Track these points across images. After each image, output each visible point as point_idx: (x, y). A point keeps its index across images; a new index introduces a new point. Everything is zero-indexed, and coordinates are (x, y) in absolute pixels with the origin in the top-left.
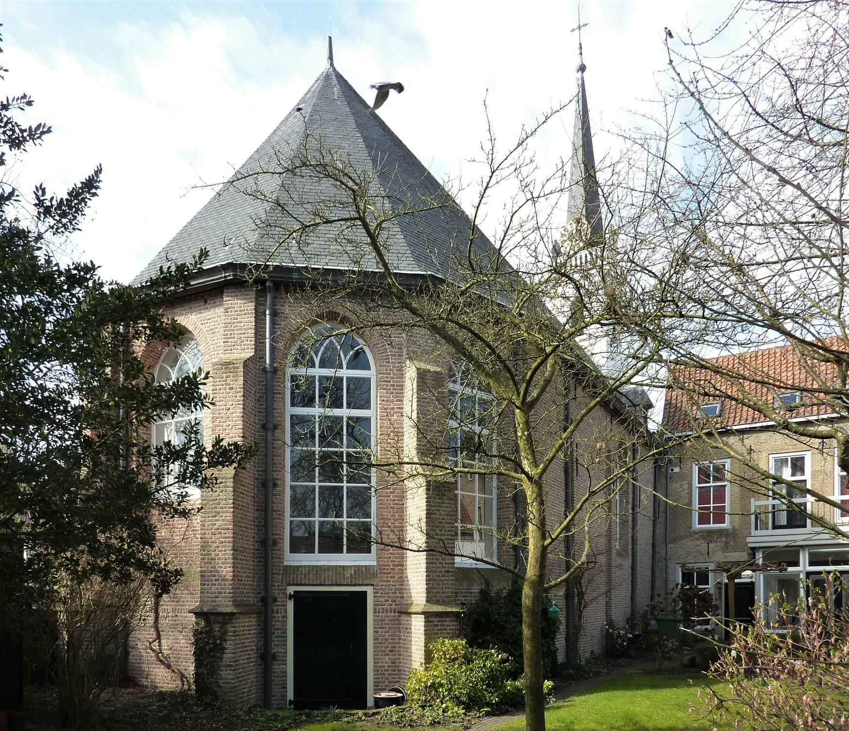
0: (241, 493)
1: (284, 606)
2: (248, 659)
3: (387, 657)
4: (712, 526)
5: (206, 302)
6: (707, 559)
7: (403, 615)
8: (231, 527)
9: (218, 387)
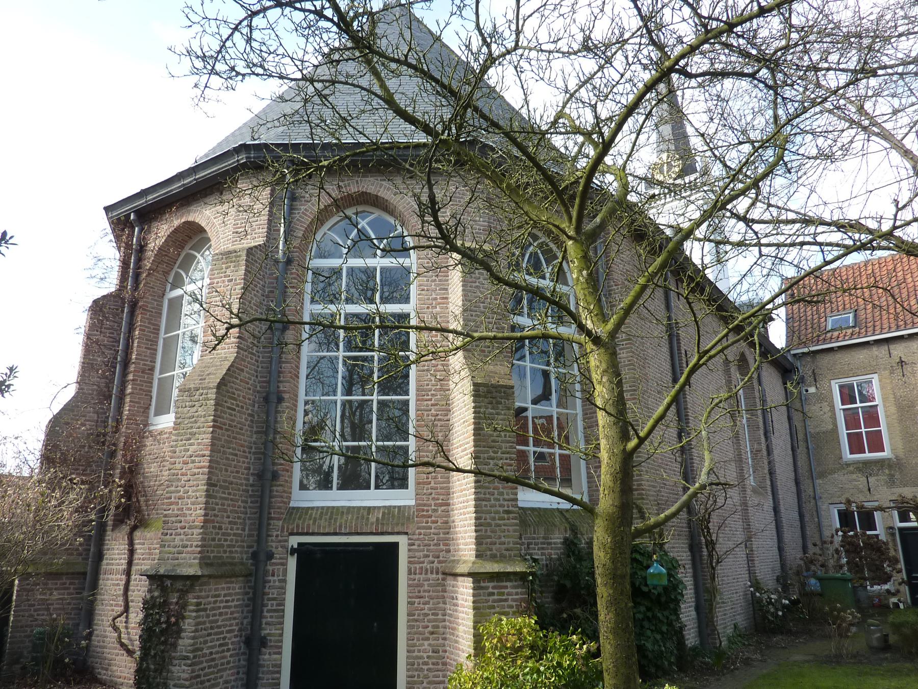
0: (229, 408)
1: (282, 564)
2: (221, 645)
3: (426, 643)
4: (868, 455)
5: (221, 194)
6: (869, 497)
7: (449, 578)
8: (208, 453)
9: (216, 281)
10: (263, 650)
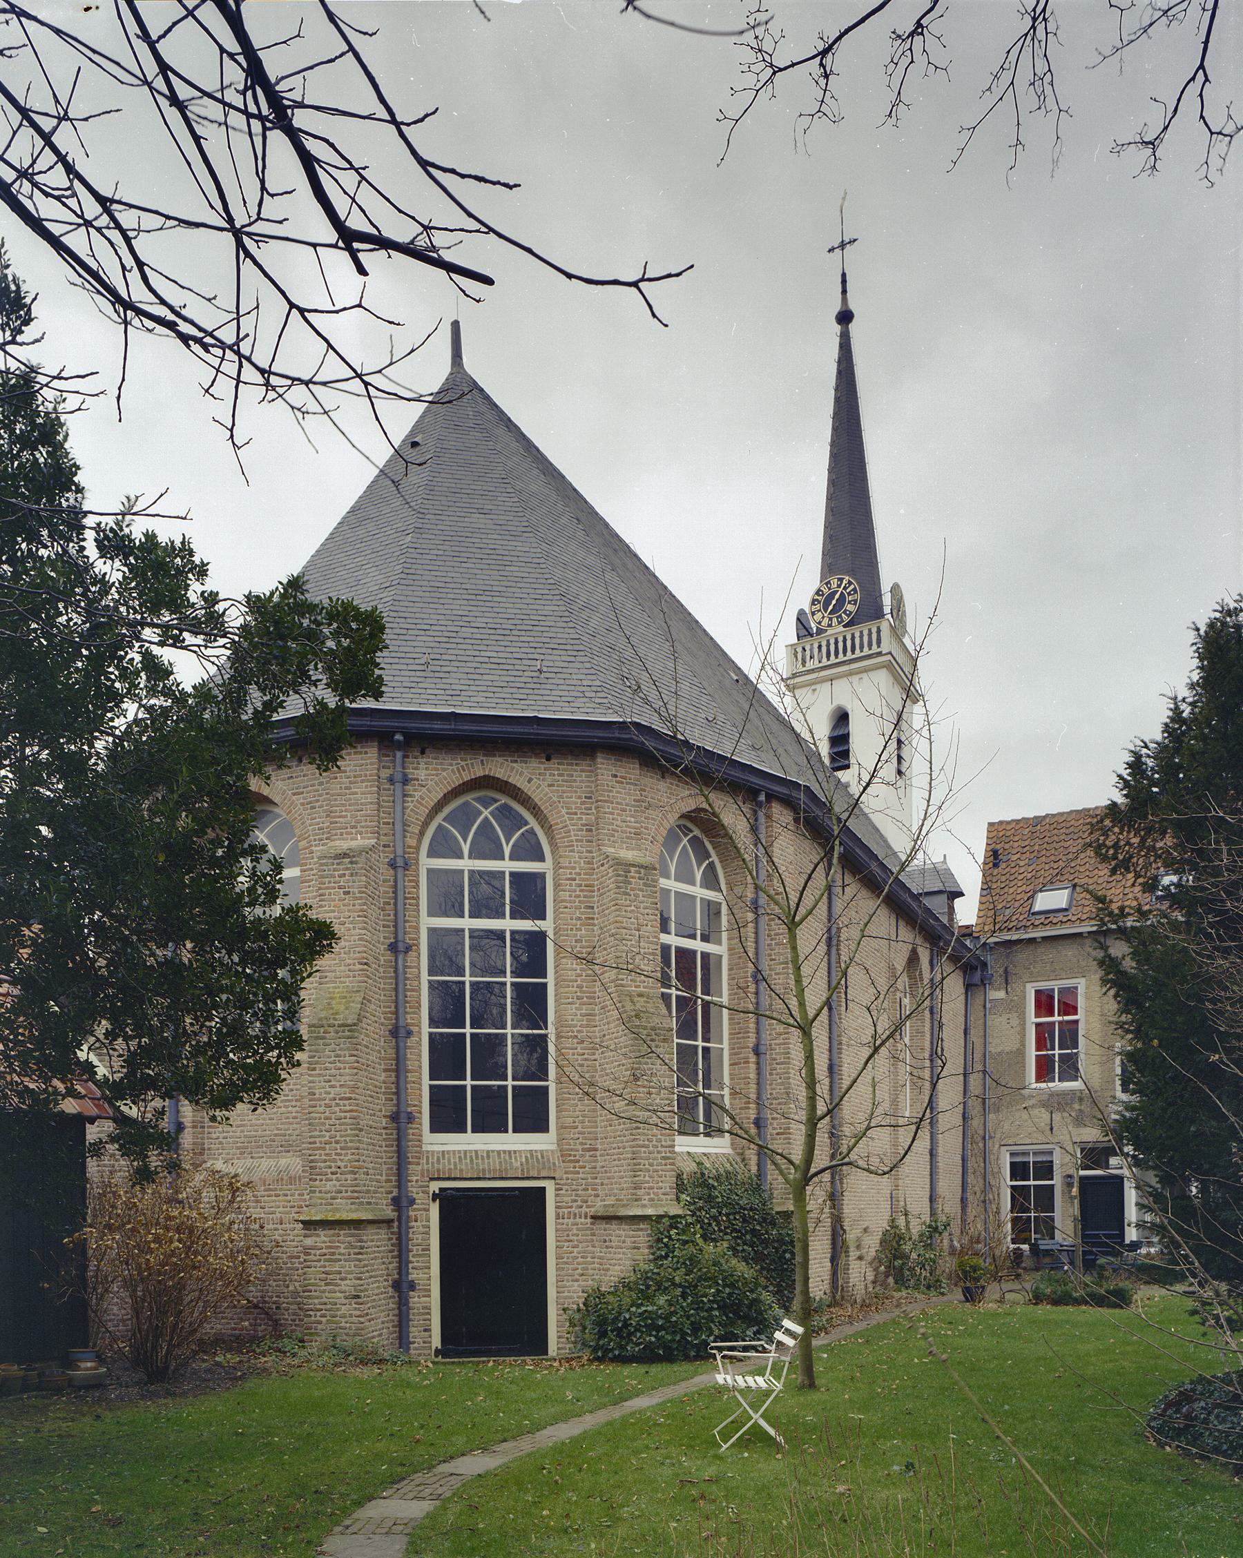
10: (411, 1293)
